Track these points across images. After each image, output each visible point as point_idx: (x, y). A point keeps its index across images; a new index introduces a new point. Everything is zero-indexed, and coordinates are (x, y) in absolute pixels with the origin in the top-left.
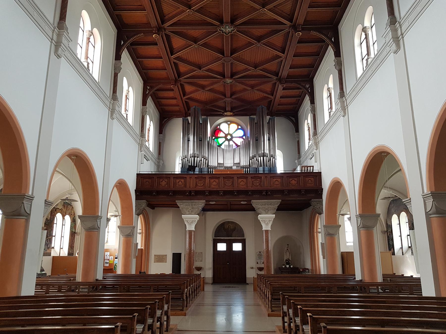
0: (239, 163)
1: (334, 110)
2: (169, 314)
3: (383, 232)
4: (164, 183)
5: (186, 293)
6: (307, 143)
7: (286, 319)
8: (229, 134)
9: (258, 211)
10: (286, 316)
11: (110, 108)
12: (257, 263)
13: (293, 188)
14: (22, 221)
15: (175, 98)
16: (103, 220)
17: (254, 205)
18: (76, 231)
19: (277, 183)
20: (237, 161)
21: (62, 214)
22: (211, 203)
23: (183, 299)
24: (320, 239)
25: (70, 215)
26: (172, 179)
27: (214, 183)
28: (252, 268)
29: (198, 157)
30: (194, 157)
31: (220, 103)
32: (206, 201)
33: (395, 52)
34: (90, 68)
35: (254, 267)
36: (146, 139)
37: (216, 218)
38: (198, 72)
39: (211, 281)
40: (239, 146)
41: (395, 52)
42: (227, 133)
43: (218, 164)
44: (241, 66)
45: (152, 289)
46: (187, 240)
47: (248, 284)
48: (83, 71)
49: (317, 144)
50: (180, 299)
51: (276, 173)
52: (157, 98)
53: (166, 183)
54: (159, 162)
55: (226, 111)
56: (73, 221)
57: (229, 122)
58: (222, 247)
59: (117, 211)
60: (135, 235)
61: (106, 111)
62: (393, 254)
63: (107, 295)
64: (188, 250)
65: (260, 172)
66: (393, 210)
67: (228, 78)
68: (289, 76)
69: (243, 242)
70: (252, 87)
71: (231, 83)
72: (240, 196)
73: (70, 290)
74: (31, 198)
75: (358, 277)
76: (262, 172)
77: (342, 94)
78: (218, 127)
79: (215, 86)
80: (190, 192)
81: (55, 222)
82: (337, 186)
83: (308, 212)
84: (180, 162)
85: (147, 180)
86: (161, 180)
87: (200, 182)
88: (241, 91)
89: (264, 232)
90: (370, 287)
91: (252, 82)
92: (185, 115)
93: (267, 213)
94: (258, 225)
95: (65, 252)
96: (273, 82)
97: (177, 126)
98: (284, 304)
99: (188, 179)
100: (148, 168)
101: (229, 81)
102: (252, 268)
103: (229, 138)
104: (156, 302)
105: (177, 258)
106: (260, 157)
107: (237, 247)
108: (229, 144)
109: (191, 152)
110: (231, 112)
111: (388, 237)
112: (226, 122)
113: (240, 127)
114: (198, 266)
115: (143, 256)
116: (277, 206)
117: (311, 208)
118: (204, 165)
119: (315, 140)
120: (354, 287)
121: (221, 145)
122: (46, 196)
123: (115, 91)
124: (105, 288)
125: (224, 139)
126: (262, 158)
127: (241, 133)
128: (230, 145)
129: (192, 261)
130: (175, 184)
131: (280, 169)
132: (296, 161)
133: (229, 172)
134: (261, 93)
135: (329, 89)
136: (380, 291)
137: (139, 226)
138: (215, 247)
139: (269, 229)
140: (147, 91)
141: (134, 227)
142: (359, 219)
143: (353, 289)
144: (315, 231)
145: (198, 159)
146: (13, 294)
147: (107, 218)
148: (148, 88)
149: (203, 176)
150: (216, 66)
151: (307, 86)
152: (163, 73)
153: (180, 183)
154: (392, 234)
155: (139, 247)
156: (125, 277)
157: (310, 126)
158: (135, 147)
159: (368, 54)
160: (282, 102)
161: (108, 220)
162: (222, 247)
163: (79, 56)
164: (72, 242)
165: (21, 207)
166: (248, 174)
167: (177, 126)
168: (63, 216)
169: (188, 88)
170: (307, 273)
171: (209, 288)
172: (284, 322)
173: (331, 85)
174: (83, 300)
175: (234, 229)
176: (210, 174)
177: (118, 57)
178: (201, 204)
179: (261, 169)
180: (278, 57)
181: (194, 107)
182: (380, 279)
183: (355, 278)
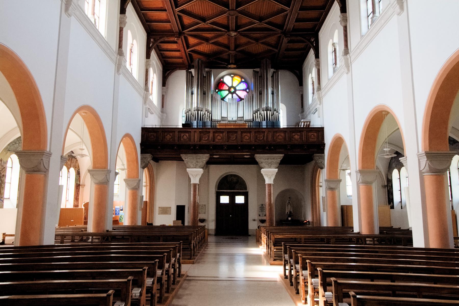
0: (243, 117)
1: (338, 66)
2: (181, 261)
3: (384, 187)
4: (168, 137)
5: (194, 244)
6: (310, 98)
7: (287, 267)
8: (232, 87)
9: (261, 165)
10: (287, 263)
12: (259, 215)
13: (296, 142)
14: (40, 176)
16: (112, 174)
17: (257, 160)
18: (81, 183)
19: (280, 137)
20: (240, 115)
21: (67, 167)
22: (215, 156)
23: (191, 248)
24: (322, 192)
25: (75, 167)
26: (177, 133)
27: (219, 138)
28: (254, 220)
29: (201, 111)
30: (198, 110)
31: (225, 56)
32: (210, 155)
33: (399, 14)
34: (97, 24)
35: (256, 218)
36: (150, 92)
37: (219, 172)
38: (202, 25)
39: (213, 233)
40: (243, 99)
41: (347, 73)
42: (230, 85)
43: (222, 117)
44: (245, 20)
45: (161, 239)
46: (192, 193)
47: (250, 235)
48: (90, 27)
49: (320, 99)
50: (188, 248)
51: (279, 128)
52: (160, 50)
53: (170, 137)
54: (162, 116)
55: (230, 64)
56: (78, 173)
58: (225, 199)
59: (124, 165)
60: (140, 188)
61: (112, 67)
62: (392, 207)
63: (114, 244)
64: (192, 203)
65: (263, 127)
66: (394, 165)
67: (233, 30)
68: (294, 30)
69: (246, 195)
70: (257, 40)
71: (235, 36)
73: (81, 240)
74: (50, 154)
75: (356, 230)
76: (265, 127)
77: (346, 51)
79: (220, 40)
80: (195, 146)
81: (61, 175)
82: (339, 142)
83: (310, 166)
84: (184, 115)
86: (166, 134)
88: (246, 44)
89: (267, 187)
90: (367, 239)
91: (257, 35)
92: (187, 67)
93: (270, 167)
94: (261, 179)
95: (70, 205)
96: (279, 35)
97: (180, 78)
98: (285, 253)
99: (192, 134)
100: (153, 122)
101: (233, 34)
102: (254, 220)
103: (232, 91)
104: (171, 250)
105: (180, 210)
106: (263, 111)
107: (240, 200)
108: (232, 97)
109: (195, 105)
110: (234, 64)
111: (388, 191)
112: (229, 74)
113: (243, 80)
114: (201, 218)
115: (147, 208)
116: (280, 160)
117: (313, 163)
119: (319, 95)
120: (351, 239)
121: (224, 98)
122: (61, 152)
123: (120, 46)
124: (114, 238)
125: (227, 92)
126: (265, 112)
127: (243, 86)
128: (234, 102)
129: (197, 213)
130: (179, 138)
131: (283, 124)
132: (300, 115)
133: (232, 127)
134: (265, 46)
135: (333, 44)
136: (376, 243)
137: (144, 180)
138: (218, 199)
139: (272, 182)
140: (150, 43)
141: (140, 181)
142: (359, 175)
143: (350, 241)
144: (317, 185)
145: (202, 112)
146: (37, 244)
147: (116, 172)
148: (152, 40)
149: (208, 130)
150: (221, 19)
152: (167, 25)
153: (185, 136)
154: (392, 188)
155: (144, 200)
156: (132, 228)
157: (314, 80)
158: (140, 100)
159: (374, 12)
160: (284, 45)
161: (117, 174)
162: (225, 199)
163: (86, 13)
164: (77, 194)
165: (40, 163)
166: (251, 129)
167: (180, 78)
168: (68, 169)
169: (192, 41)
170: (307, 226)
171: (211, 239)
172: (285, 269)
173: (336, 40)
174: (97, 249)
175: (237, 183)
176: (214, 128)
177: (123, 11)
178: (205, 157)
179: (264, 123)
180: (283, 10)
182: (377, 232)
183: (353, 231)
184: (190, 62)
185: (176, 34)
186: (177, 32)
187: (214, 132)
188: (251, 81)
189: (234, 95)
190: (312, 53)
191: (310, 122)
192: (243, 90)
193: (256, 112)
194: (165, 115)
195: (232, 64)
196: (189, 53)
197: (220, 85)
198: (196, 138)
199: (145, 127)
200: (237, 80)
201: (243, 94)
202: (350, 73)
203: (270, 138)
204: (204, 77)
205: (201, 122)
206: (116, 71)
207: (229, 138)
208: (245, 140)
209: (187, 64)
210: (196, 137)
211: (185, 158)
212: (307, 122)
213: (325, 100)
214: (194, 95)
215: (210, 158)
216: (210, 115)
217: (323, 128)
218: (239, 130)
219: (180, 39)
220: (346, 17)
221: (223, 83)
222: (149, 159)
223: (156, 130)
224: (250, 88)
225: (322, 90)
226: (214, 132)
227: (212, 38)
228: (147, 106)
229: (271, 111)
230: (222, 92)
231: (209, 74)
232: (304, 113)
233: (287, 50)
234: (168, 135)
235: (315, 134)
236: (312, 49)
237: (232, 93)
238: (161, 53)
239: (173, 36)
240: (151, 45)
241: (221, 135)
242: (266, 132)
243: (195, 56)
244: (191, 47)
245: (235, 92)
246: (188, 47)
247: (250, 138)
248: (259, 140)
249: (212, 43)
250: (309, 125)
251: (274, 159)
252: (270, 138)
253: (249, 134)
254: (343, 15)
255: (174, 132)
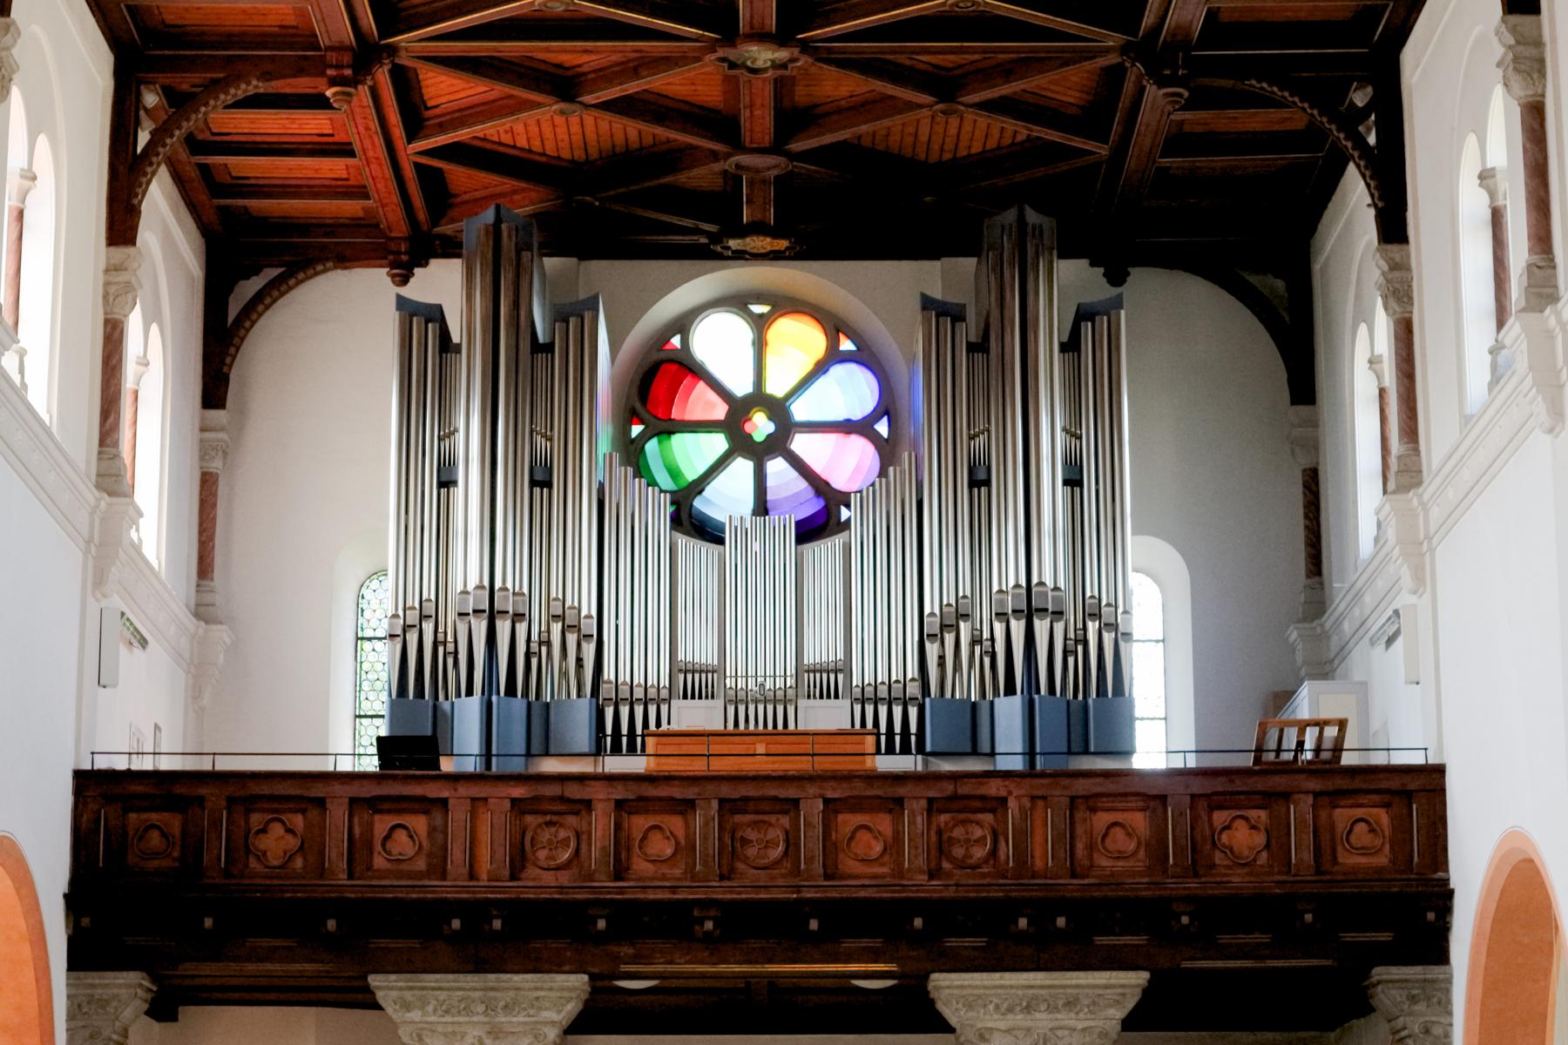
4: (276, 842)
6: (1364, 505)
8: (759, 399)
11: (89, 542)
15: (345, 150)
19: (1119, 840)
26: (338, 813)
29: (518, 617)
32: (593, 977)
42: (741, 386)
53: (292, 842)
55: (743, 232)
57: (760, 298)
71: (776, 66)
72: (849, 944)
76: (1017, 764)
78: (676, 341)
79: (671, 83)
80: (476, 911)
85: (154, 817)
86: (256, 819)
87: (546, 835)
96: (1102, 62)
97: (342, 332)
99: (458, 814)
101: (763, 55)
106: (1001, 615)
110: (774, 233)
112: (737, 302)
113: (846, 345)
118: (564, 674)
125: (718, 443)
127: (851, 392)
130: (359, 849)
135: (1486, 177)
140: (137, 123)
148: (151, 99)
151: (1360, 98)
153: (403, 842)
158: (63, 563)
169: (444, 89)
181: (489, 215)
184: (422, 215)
185: (332, 57)
186: (340, 48)
187: (620, 805)
188: (911, 361)
189: (777, 468)
190: (1355, 195)
191: (1342, 724)
192: (846, 427)
193: (948, 626)
194: (221, 633)
195: (758, 228)
196: (417, 166)
197: (659, 381)
198: (484, 854)
199: (102, 763)
200: (797, 342)
201: (848, 463)
202: (1427, 596)
203: (1043, 853)
204: (537, 348)
205: (518, 704)
206: (89, 585)
207: (731, 852)
208: (849, 865)
209: (401, 229)
210: (489, 840)
211: (407, 1007)
212: (1321, 724)
213: (1448, 560)
214: (458, 492)
215: (595, 991)
216: (589, 650)
217: (1439, 770)
218: (812, 790)
219: (364, 90)
220: (1539, 43)
221: (690, 369)
222: (128, 1013)
223: (180, 790)
224: (904, 413)
225: (1429, 489)
226: (620, 805)
227: (606, 75)
228: (116, 602)
229: (1058, 614)
230: (681, 443)
231: (574, 315)
232: (1328, 621)
233: (1178, 141)
234: (277, 830)
235: (1383, 817)
236: (1351, 167)
237: (759, 453)
238: (205, 169)
239: (316, 66)
240: (143, 138)
241: (675, 823)
242: (1012, 804)
243: (460, 177)
244: (442, 128)
245: (777, 445)
246: (416, 122)
247: (893, 846)
248: (961, 865)
249: (606, 106)
250: (1338, 749)
251: (1071, 1004)
252: (1043, 853)
253: (884, 823)
254: (1513, 30)
255: (320, 803)
